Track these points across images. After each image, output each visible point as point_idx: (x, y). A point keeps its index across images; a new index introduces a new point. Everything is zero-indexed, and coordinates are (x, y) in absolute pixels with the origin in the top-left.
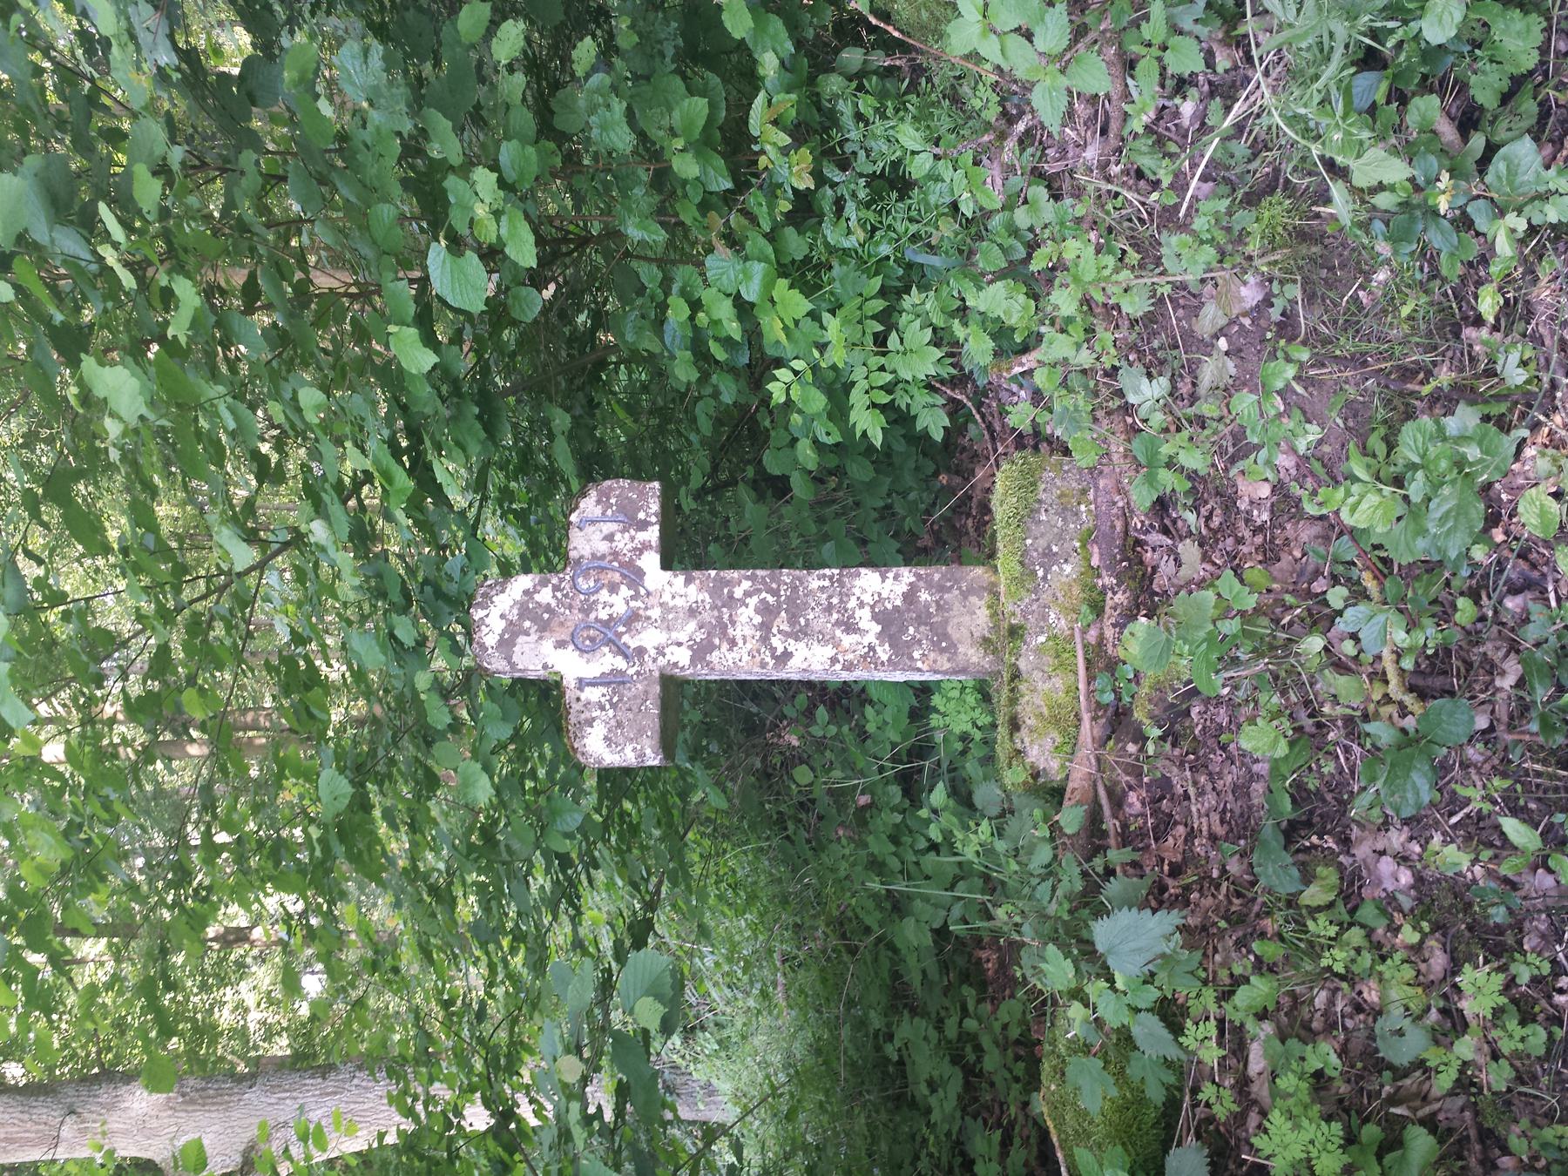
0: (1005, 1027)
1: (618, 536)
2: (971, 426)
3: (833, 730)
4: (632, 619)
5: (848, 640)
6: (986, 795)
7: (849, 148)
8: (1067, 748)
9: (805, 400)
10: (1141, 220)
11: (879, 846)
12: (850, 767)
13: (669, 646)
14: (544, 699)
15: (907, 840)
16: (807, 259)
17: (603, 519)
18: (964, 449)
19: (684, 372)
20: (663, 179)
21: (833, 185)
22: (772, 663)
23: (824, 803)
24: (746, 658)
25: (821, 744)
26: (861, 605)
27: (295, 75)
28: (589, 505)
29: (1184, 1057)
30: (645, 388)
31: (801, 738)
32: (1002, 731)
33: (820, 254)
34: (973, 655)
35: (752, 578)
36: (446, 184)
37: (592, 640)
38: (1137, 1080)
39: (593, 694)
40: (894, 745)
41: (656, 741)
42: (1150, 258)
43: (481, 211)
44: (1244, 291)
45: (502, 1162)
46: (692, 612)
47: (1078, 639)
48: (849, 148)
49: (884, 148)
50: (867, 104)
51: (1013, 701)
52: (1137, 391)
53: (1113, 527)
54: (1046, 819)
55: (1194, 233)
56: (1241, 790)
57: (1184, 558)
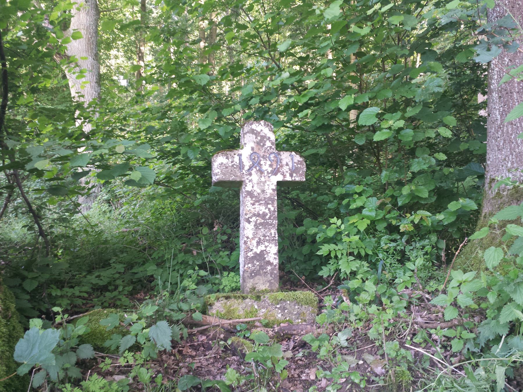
0: (120, 300)
1: (288, 167)
2: (321, 287)
3: (219, 241)
4: (261, 172)
5: (254, 242)
6: (203, 289)
7: (413, 243)
9: (331, 230)
10: (399, 335)
13: (252, 184)
14: (234, 144)
15: (183, 267)
16: (376, 230)
19: (338, 191)
20: (400, 184)
21: (401, 239)
23: (194, 240)
24: (248, 209)
26: (266, 247)
27: (432, 65)
28: (297, 158)
29: (120, 353)
30: (325, 184)
32: (225, 294)
33: (378, 234)
34: (249, 284)
35: (274, 211)
36: (399, 112)
37: (254, 159)
38: (111, 337)
39: (236, 159)
42: (390, 337)
43: (391, 122)
44: (380, 368)
45: (73, 136)
46: (263, 191)
47: (257, 318)
48: (413, 243)
49: (414, 255)
50: (428, 248)
51: (235, 297)
52: (344, 334)
53: (294, 330)
54: (197, 308)
55: (399, 350)
56: (209, 372)
57: (286, 353)
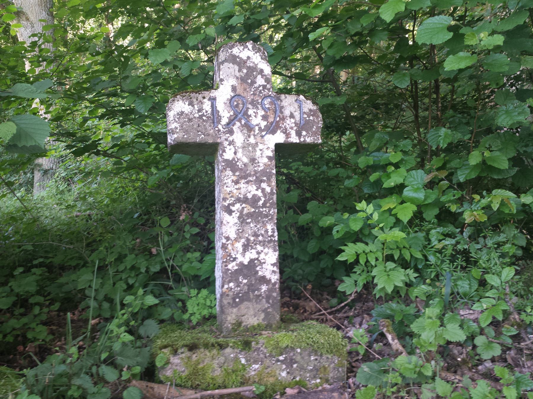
1: (293, 120)
3: (188, 236)
4: (249, 128)
5: (239, 246)
8: (179, 381)
9: (355, 220)
11: (129, 261)
12: (168, 246)
15: (133, 274)
17: (302, 113)
18: (322, 295)
19: (363, 161)
21: (462, 232)
22: (226, 204)
24: (228, 190)
25: (180, 230)
28: (308, 105)
31: (184, 220)
32: (188, 337)
34: (231, 317)
35: (272, 193)
37: (237, 106)
39: (207, 106)
40: (180, 267)
41: (181, 140)
46: (253, 160)
48: (481, 240)
51: (207, 346)
